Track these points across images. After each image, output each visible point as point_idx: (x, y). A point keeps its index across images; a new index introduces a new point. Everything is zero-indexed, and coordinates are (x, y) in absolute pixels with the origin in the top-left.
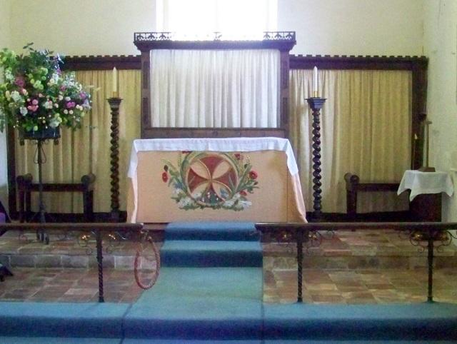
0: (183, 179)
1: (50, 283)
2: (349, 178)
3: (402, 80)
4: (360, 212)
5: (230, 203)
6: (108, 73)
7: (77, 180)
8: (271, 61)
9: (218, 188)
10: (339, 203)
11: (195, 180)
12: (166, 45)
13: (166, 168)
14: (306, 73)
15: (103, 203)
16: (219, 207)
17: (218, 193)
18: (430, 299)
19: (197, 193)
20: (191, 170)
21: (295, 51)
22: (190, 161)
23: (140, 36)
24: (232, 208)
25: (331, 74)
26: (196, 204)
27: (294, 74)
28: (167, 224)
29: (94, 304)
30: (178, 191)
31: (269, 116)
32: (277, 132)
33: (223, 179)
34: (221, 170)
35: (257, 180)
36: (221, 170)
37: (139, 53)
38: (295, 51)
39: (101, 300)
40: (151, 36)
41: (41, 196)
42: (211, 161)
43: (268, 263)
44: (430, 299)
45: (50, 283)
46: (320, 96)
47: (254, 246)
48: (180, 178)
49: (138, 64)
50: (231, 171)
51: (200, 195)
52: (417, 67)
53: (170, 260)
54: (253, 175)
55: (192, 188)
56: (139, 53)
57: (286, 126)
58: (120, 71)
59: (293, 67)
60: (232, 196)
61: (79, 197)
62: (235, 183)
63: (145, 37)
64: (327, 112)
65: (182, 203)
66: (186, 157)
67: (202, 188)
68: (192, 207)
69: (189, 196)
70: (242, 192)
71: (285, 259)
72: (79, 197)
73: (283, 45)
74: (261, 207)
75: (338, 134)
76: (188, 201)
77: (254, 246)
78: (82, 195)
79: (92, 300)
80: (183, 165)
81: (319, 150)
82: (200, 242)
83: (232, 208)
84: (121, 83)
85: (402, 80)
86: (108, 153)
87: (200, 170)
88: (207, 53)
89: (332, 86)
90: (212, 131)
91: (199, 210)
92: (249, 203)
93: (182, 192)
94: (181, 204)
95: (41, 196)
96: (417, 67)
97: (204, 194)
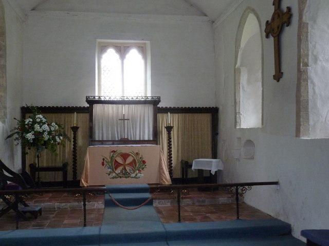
0: (112, 165)
1: (54, 217)
2: (184, 162)
3: (206, 118)
4: (190, 177)
5: (133, 175)
6: (72, 115)
7: (60, 165)
8: (149, 111)
9: (128, 168)
10: (19, 171)
11: (117, 165)
12: (100, 102)
13: (104, 159)
14: (165, 115)
15: (70, 177)
16: (128, 177)
17: (128, 171)
18: (238, 218)
19: (118, 171)
20: (116, 161)
21: (160, 105)
22: (115, 156)
23: (89, 98)
24: (135, 177)
25: (176, 116)
26: (118, 176)
27: (160, 116)
28: (104, 186)
29: (81, 228)
30: (109, 170)
31: (148, 135)
32: (153, 142)
33: (130, 164)
34: (130, 160)
35: (146, 164)
36: (130, 160)
37: (88, 105)
38: (160, 105)
39: (85, 225)
40: (99, 98)
41: (39, 173)
42: (125, 156)
43: (156, 203)
44: (238, 218)
45: (54, 217)
46: (172, 125)
47: (147, 195)
48: (110, 164)
49: (89, 111)
50: (134, 160)
51: (119, 172)
52: (214, 112)
53: (109, 204)
54: (144, 162)
55: (116, 168)
56: (88, 105)
57: (156, 139)
58: (79, 114)
59: (159, 113)
60: (134, 172)
61: (60, 173)
62: (136, 165)
63: (91, 98)
64: (174, 133)
65: (111, 176)
66: (113, 155)
67: (121, 168)
68: (116, 178)
69: (115, 172)
70: (139, 171)
71: (163, 201)
72: (60, 173)
73: (154, 102)
74: (144, 178)
75: (180, 143)
76: (114, 174)
77: (147, 195)
78: (62, 173)
79: (79, 226)
80: (112, 158)
81: (171, 151)
82: (132, 194)
83: (135, 177)
84: (76, 119)
85: (206, 118)
86: (72, 153)
87: (119, 160)
88: (120, 106)
89: (177, 120)
90: (111, 142)
91: (119, 179)
92: (142, 175)
93: (111, 170)
94: (111, 176)
95: (39, 173)
96: (214, 112)
97: (122, 171)
